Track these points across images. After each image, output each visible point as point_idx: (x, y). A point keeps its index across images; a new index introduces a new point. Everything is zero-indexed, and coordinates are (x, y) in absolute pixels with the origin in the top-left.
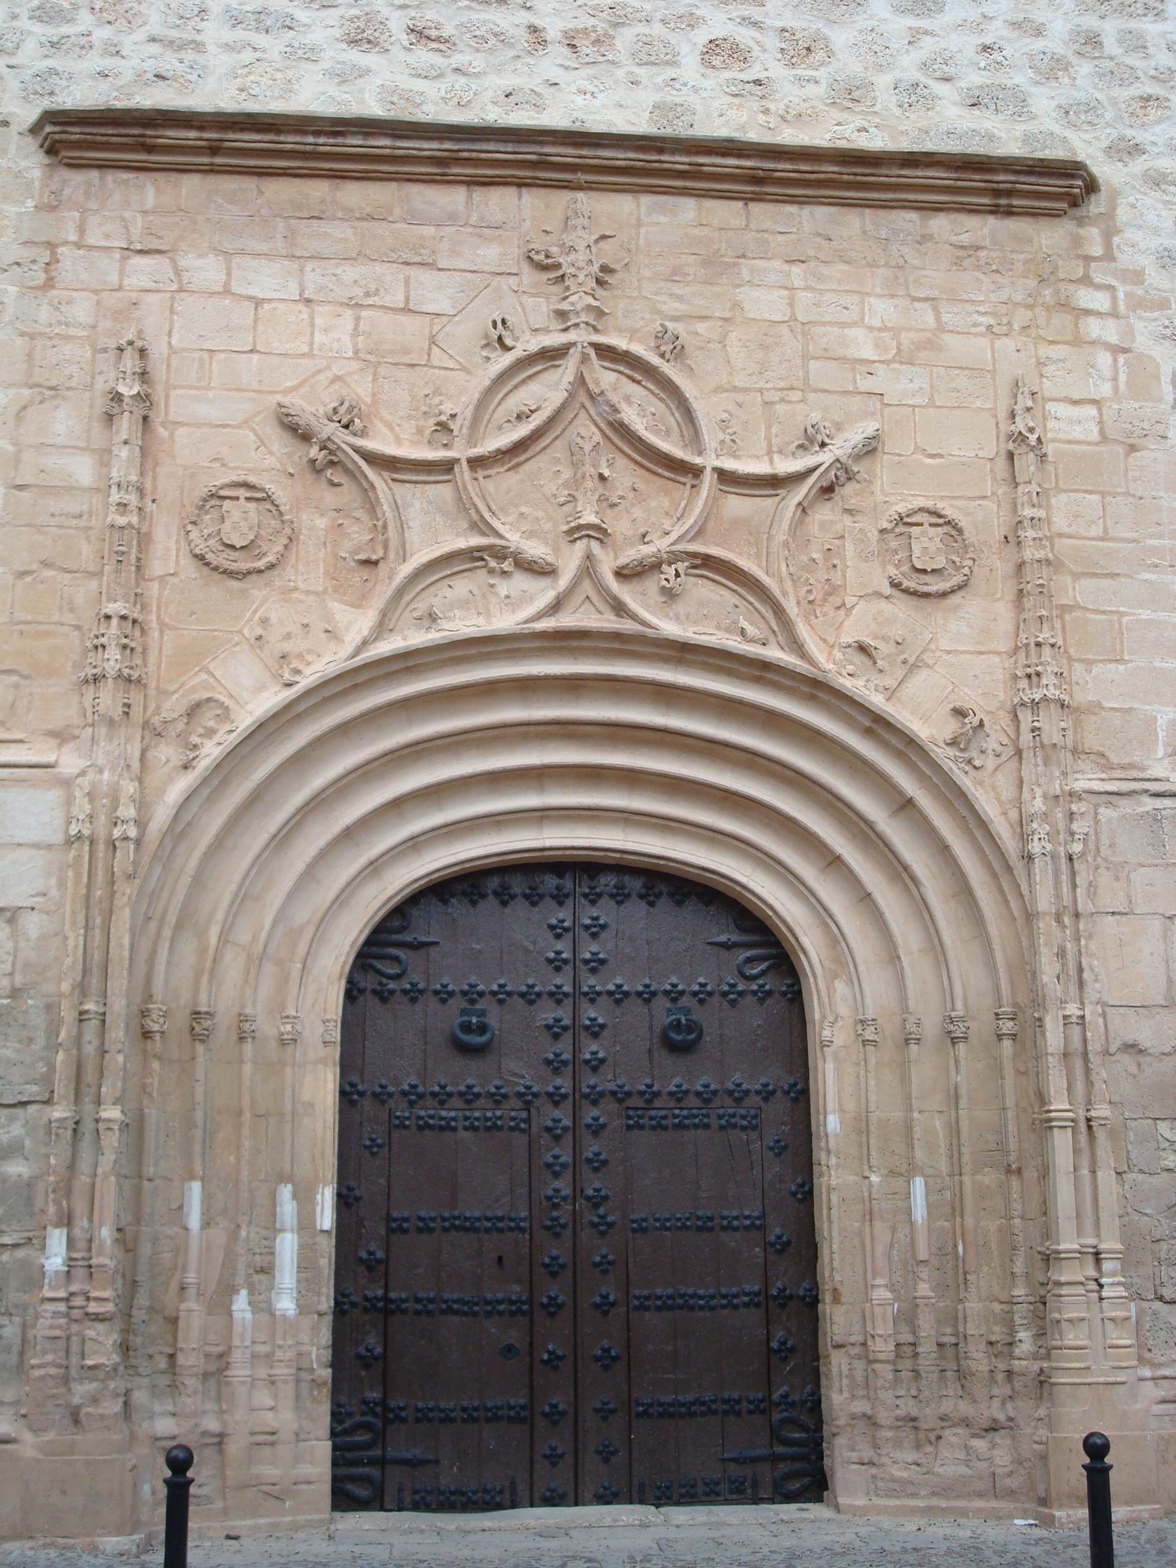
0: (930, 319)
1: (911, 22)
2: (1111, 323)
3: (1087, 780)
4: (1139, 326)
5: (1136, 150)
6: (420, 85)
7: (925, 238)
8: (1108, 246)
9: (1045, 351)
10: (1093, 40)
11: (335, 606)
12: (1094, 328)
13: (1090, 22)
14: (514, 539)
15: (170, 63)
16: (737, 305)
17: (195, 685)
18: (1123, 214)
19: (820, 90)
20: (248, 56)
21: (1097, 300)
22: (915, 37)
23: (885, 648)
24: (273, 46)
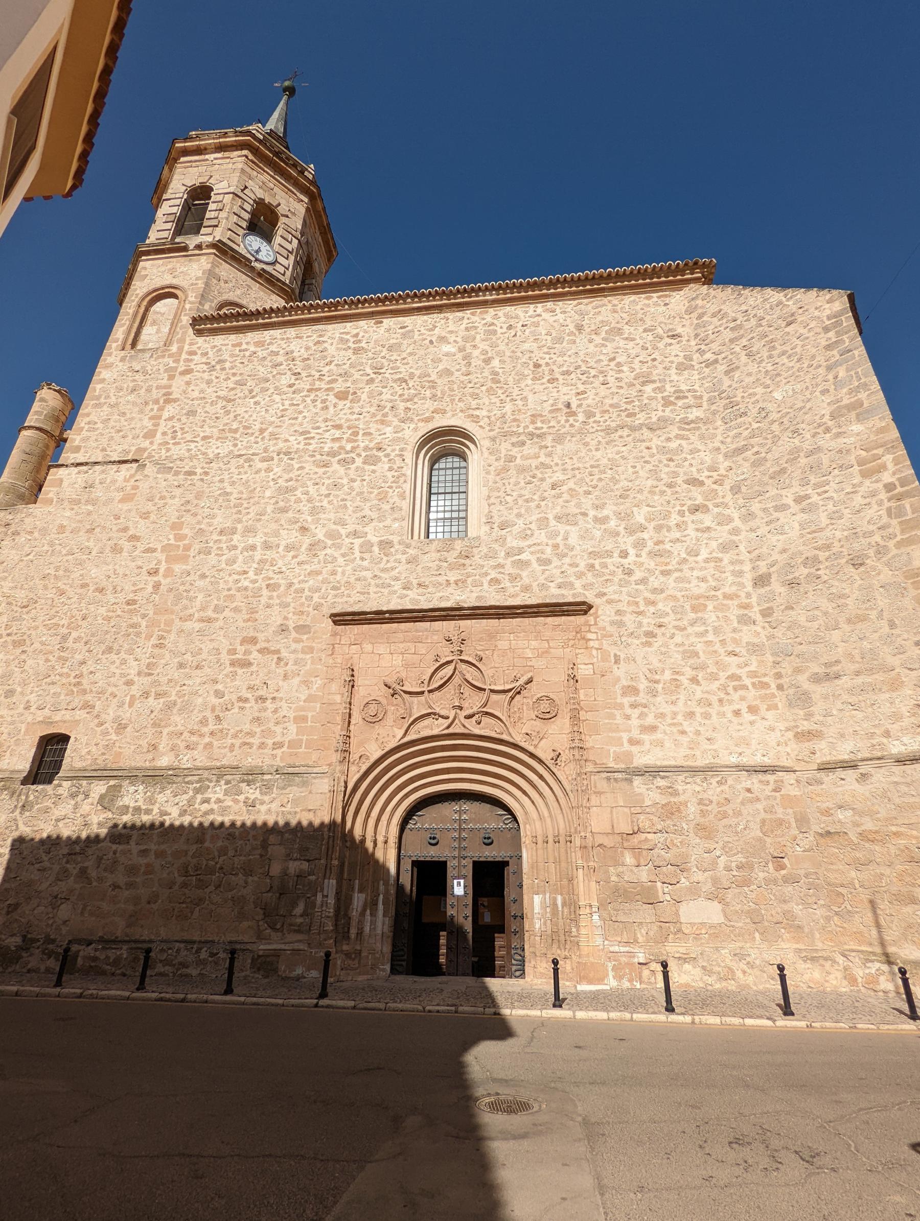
0: (547, 646)
1: (543, 568)
2: (597, 642)
3: (590, 768)
4: (604, 642)
5: (605, 594)
6: (420, 597)
7: (545, 624)
8: (596, 621)
9: (578, 651)
10: (593, 566)
11: (395, 729)
12: (591, 644)
13: (592, 561)
14: (437, 710)
15: (362, 598)
16: (496, 646)
17: (361, 751)
18: (600, 612)
19: (518, 588)
20: (380, 594)
21: (590, 636)
22: (544, 571)
23: (534, 734)
24: (386, 591)
